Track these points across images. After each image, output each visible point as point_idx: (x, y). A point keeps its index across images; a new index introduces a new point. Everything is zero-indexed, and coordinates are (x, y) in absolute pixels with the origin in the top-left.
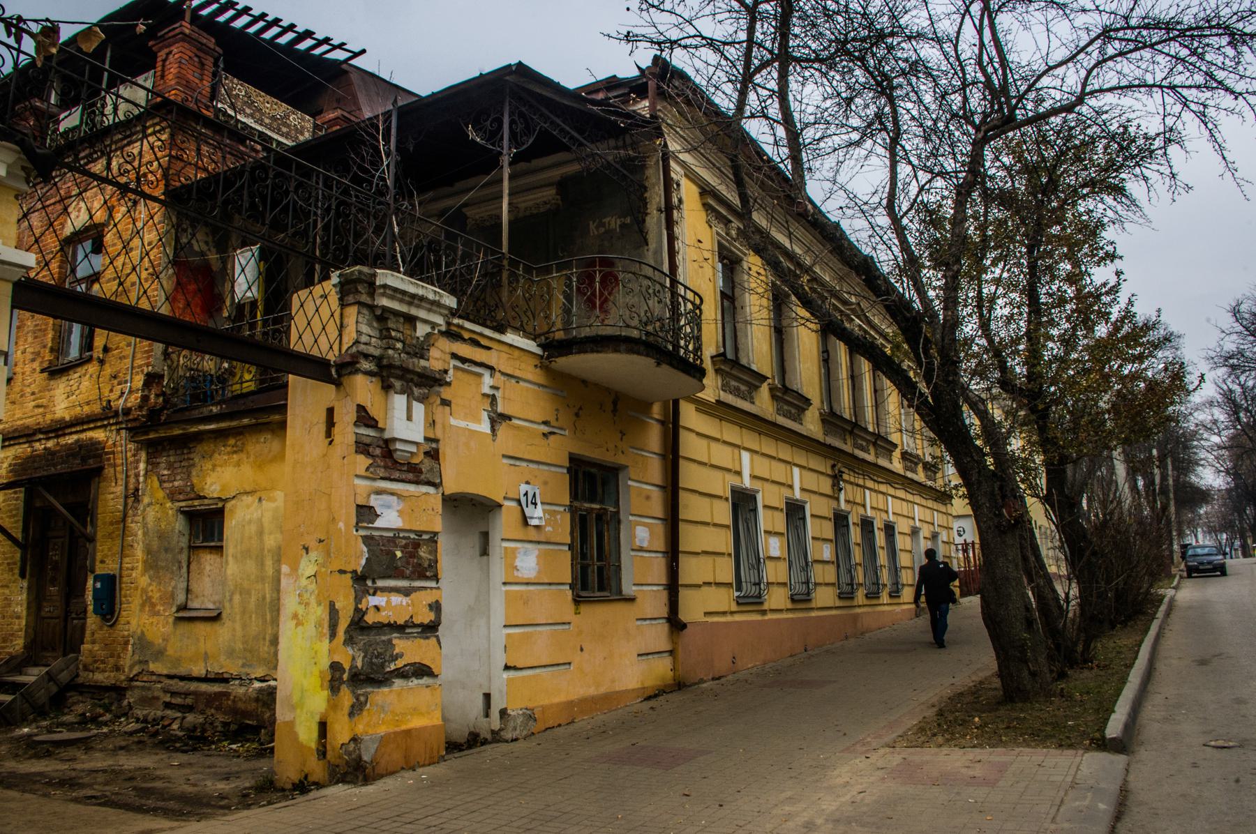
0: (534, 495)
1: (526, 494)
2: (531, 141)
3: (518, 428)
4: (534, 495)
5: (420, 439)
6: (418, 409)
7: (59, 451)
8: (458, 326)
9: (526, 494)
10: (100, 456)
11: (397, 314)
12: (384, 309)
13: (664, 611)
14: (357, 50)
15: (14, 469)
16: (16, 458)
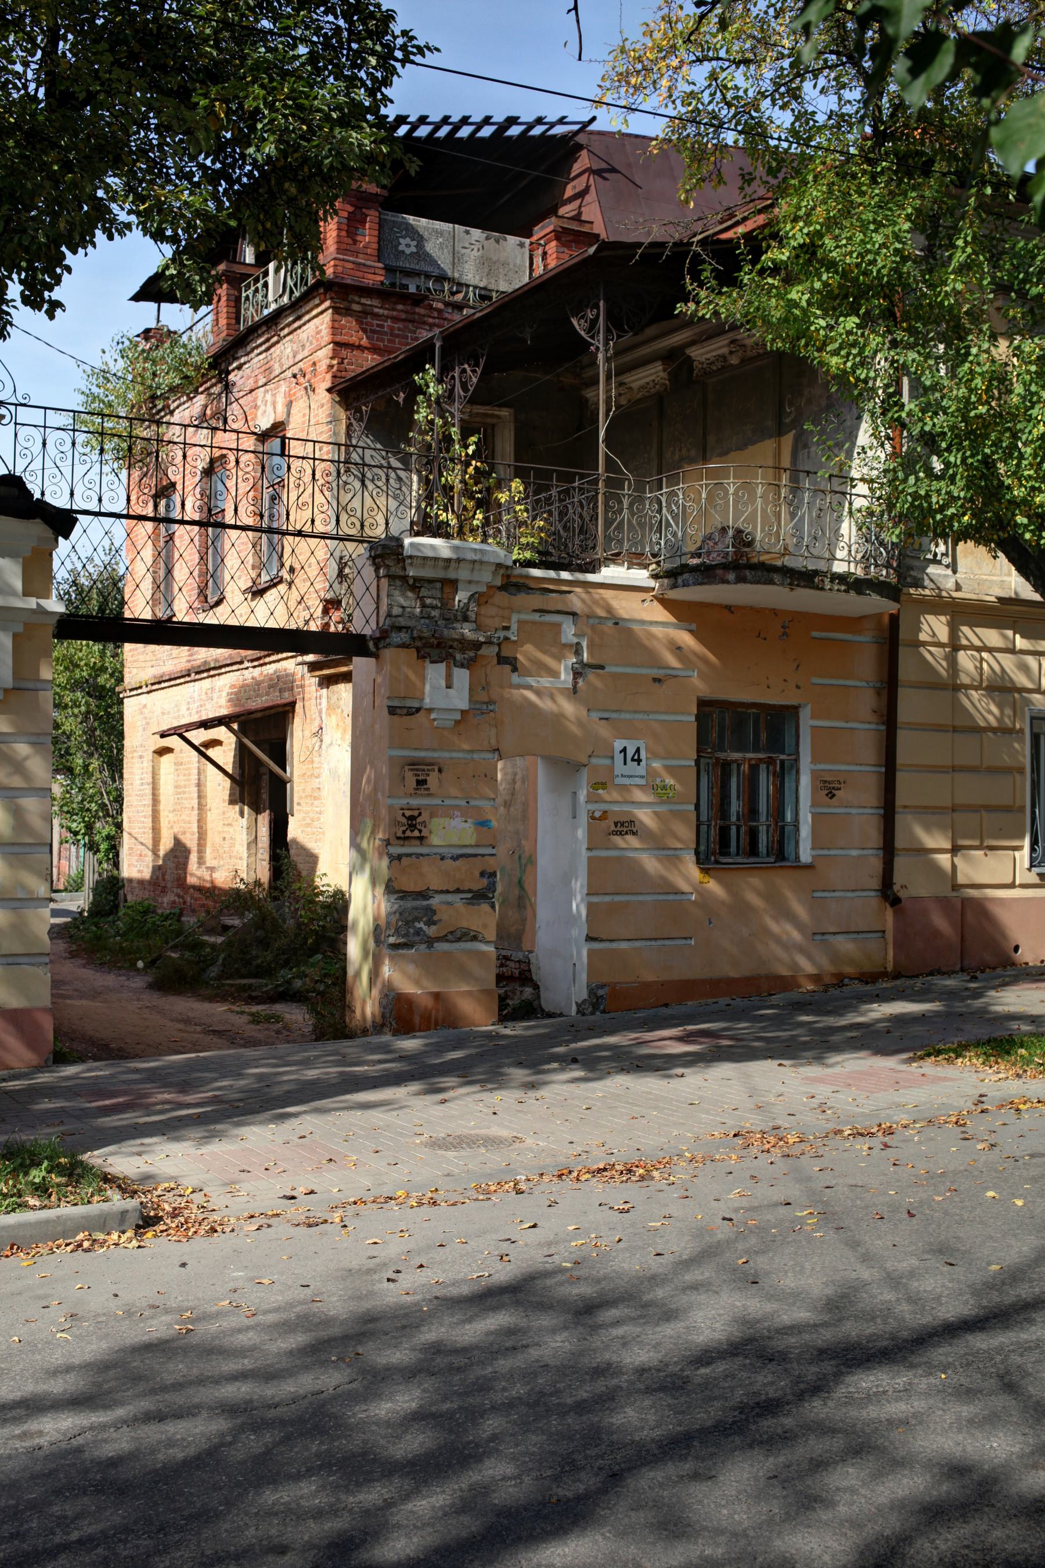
0: (638, 750)
1: (624, 750)
2: (582, 333)
3: (615, 676)
4: (638, 750)
5: (464, 705)
6: (462, 677)
7: (263, 681)
8: (521, 576)
9: (624, 750)
10: (292, 689)
11: (430, 581)
12: (416, 579)
13: (875, 883)
14: (587, 119)
15: (239, 694)
16: (232, 686)
